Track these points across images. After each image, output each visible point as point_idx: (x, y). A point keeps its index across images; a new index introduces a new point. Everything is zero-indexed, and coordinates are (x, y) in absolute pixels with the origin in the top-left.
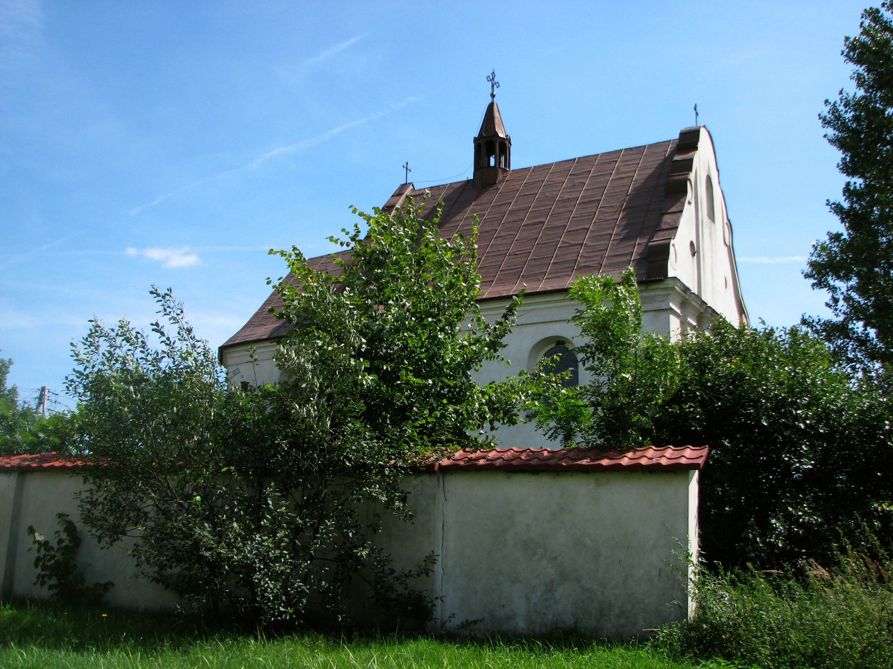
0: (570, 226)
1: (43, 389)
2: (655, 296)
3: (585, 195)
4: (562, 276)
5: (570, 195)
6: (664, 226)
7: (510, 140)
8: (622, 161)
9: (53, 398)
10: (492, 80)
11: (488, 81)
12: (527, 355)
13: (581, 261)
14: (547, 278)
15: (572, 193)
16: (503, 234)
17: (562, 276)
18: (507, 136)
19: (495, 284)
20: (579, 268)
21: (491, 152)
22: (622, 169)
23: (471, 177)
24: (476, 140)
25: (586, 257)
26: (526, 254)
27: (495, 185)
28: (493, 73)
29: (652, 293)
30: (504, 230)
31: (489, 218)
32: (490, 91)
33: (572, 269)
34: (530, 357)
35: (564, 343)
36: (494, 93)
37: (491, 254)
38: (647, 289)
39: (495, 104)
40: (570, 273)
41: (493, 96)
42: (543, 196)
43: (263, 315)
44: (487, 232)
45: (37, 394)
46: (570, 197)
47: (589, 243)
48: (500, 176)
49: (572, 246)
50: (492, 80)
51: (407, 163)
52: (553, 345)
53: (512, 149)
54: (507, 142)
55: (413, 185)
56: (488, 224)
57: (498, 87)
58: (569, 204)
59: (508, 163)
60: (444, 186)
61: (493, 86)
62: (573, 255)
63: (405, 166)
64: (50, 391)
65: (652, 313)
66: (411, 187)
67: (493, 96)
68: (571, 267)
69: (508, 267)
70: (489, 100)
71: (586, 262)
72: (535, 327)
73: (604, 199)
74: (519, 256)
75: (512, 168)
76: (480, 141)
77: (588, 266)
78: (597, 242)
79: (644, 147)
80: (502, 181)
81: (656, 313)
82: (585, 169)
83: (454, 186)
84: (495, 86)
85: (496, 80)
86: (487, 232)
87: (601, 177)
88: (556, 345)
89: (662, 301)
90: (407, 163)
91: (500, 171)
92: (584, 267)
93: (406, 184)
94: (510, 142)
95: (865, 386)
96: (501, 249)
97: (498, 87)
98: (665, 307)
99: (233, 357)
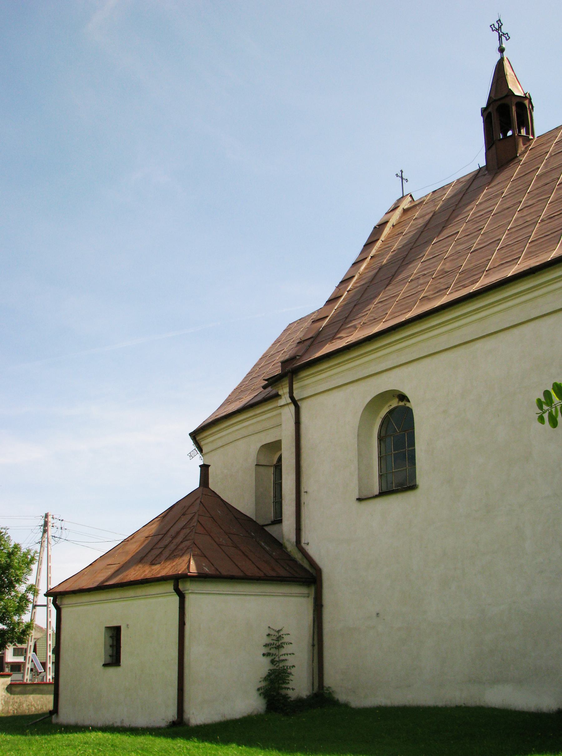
1: (47, 516)
7: (530, 99)
9: (58, 524)
10: (498, 28)
11: (493, 30)
21: (506, 126)
23: (483, 163)
24: (484, 111)
27: (517, 158)
28: (499, 20)
30: (532, 198)
31: (510, 194)
36: (504, 46)
41: (501, 50)
43: (242, 389)
45: (42, 522)
50: (498, 28)
51: (402, 171)
54: (526, 102)
55: (411, 196)
56: (508, 200)
57: (507, 40)
59: (530, 130)
60: (449, 185)
61: (500, 37)
63: (400, 174)
64: (54, 517)
66: (409, 199)
67: (501, 50)
70: (498, 57)
74: (556, 217)
75: (537, 134)
76: (490, 110)
80: (524, 152)
84: (503, 38)
85: (504, 30)
90: (402, 171)
94: (530, 102)
95: (258, 540)
96: (528, 220)
97: (507, 40)
99: (207, 443)
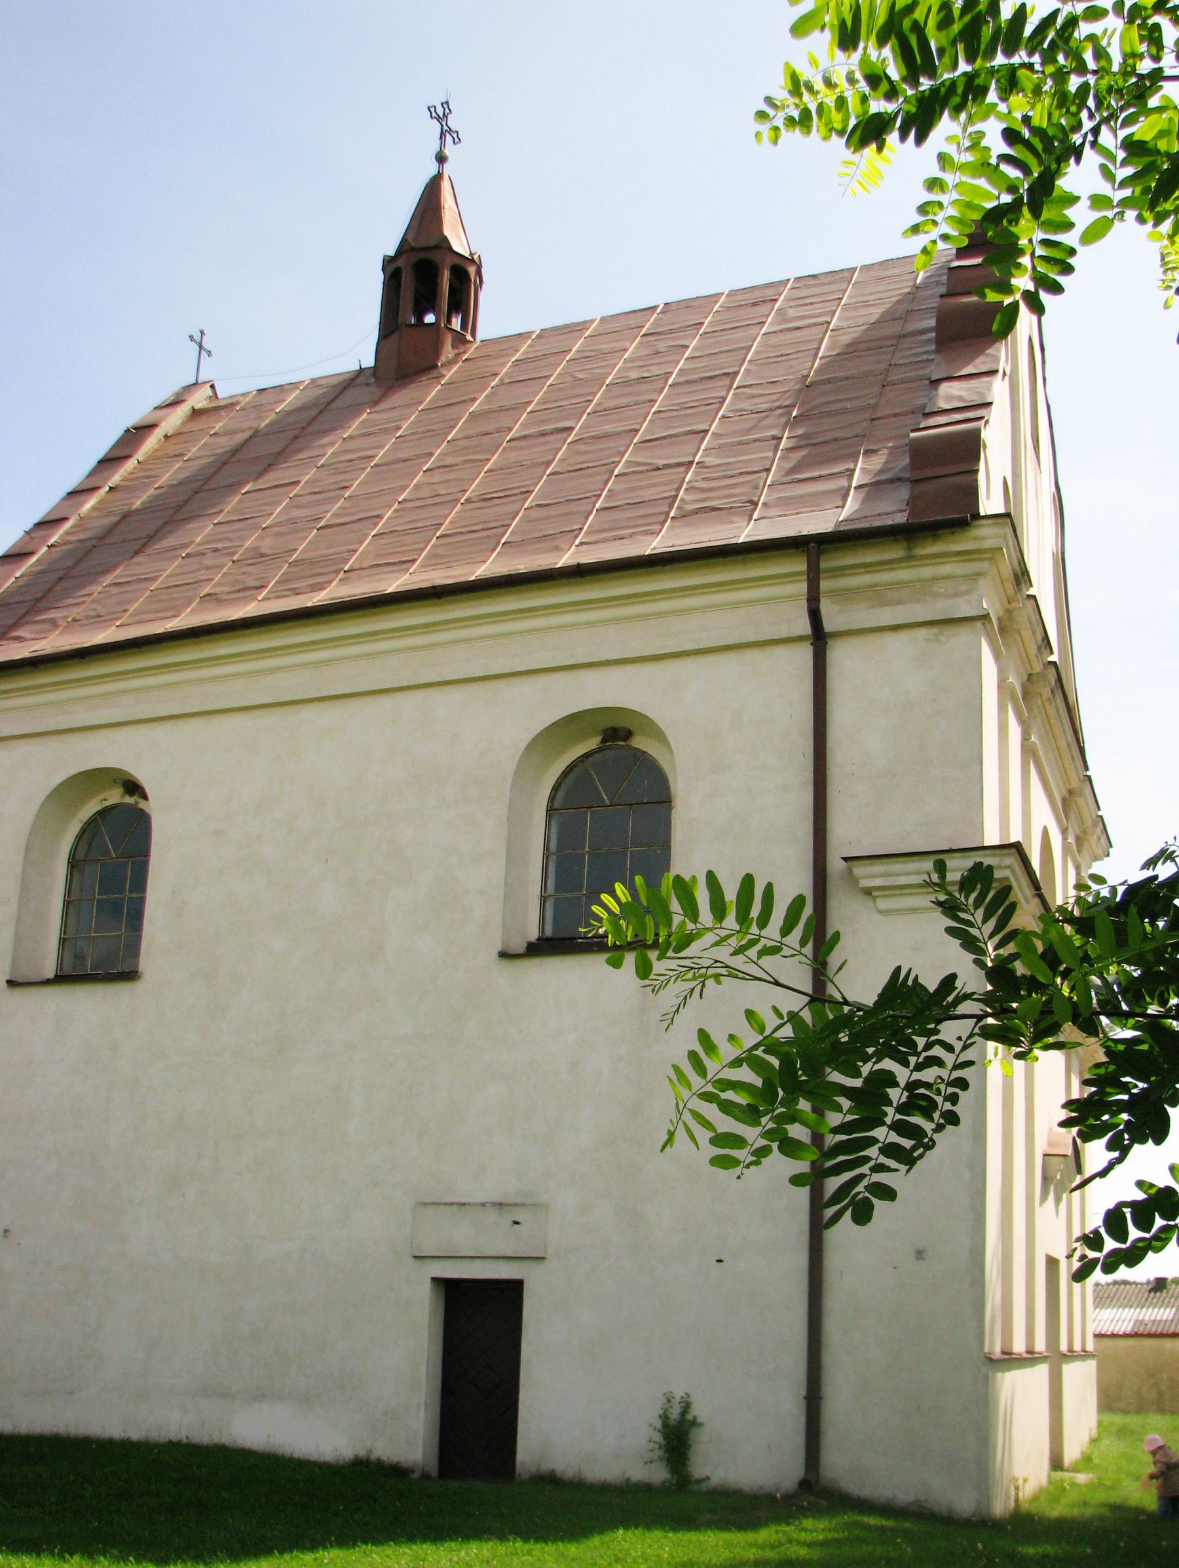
0: (648, 430)
2: (935, 579)
3: (685, 367)
4: (631, 535)
5: (648, 371)
6: (1053, 172)
8: (787, 300)
10: (441, 115)
12: (511, 766)
13: (688, 498)
14: (581, 544)
15: (652, 368)
16: (449, 460)
17: (631, 535)
18: (471, 254)
19: (422, 566)
20: (683, 516)
22: (792, 313)
23: (369, 361)
24: (388, 262)
25: (703, 490)
26: (520, 497)
29: (927, 572)
32: (435, 147)
33: (662, 518)
34: (519, 773)
35: (629, 734)
37: (411, 505)
38: (910, 558)
39: (446, 177)
40: (657, 527)
41: (441, 159)
42: (569, 379)
44: (405, 461)
46: (646, 375)
47: (710, 461)
48: (448, 352)
49: (658, 469)
50: (441, 115)
52: (593, 743)
53: (483, 295)
54: (472, 270)
55: (212, 386)
56: (407, 444)
58: (644, 387)
59: (469, 324)
61: (442, 134)
62: (668, 488)
65: (922, 633)
67: (441, 159)
68: (663, 513)
69: (463, 527)
70: (432, 169)
71: (705, 500)
72: (542, 679)
73: (747, 371)
74: (496, 501)
75: (480, 336)
77: (714, 509)
78: (737, 456)
79: (853, 270)
81: (935, 630)
82: (686, 321)
83: (321, 382)
86: (405, 461)
87: (734, 331)
88: (604, 741)
89: (957, 595)
91: (448, 340)
92: (697, 511)
93: (195, 384)
94: (479, 273)
98: (966, 611)
